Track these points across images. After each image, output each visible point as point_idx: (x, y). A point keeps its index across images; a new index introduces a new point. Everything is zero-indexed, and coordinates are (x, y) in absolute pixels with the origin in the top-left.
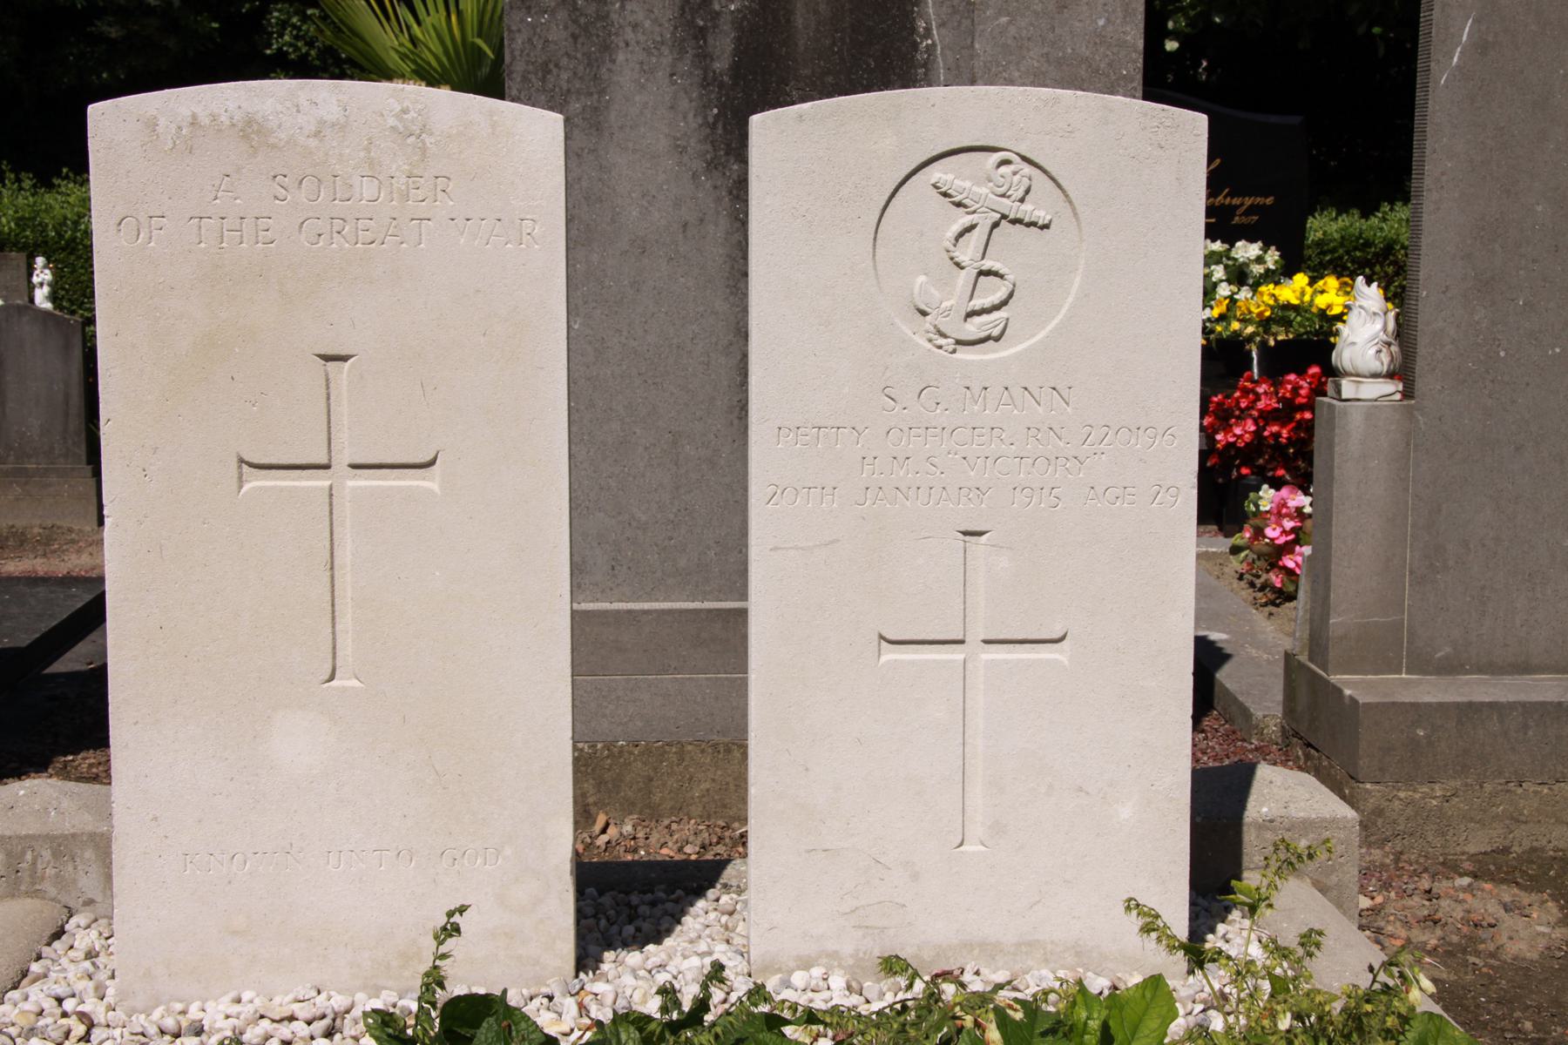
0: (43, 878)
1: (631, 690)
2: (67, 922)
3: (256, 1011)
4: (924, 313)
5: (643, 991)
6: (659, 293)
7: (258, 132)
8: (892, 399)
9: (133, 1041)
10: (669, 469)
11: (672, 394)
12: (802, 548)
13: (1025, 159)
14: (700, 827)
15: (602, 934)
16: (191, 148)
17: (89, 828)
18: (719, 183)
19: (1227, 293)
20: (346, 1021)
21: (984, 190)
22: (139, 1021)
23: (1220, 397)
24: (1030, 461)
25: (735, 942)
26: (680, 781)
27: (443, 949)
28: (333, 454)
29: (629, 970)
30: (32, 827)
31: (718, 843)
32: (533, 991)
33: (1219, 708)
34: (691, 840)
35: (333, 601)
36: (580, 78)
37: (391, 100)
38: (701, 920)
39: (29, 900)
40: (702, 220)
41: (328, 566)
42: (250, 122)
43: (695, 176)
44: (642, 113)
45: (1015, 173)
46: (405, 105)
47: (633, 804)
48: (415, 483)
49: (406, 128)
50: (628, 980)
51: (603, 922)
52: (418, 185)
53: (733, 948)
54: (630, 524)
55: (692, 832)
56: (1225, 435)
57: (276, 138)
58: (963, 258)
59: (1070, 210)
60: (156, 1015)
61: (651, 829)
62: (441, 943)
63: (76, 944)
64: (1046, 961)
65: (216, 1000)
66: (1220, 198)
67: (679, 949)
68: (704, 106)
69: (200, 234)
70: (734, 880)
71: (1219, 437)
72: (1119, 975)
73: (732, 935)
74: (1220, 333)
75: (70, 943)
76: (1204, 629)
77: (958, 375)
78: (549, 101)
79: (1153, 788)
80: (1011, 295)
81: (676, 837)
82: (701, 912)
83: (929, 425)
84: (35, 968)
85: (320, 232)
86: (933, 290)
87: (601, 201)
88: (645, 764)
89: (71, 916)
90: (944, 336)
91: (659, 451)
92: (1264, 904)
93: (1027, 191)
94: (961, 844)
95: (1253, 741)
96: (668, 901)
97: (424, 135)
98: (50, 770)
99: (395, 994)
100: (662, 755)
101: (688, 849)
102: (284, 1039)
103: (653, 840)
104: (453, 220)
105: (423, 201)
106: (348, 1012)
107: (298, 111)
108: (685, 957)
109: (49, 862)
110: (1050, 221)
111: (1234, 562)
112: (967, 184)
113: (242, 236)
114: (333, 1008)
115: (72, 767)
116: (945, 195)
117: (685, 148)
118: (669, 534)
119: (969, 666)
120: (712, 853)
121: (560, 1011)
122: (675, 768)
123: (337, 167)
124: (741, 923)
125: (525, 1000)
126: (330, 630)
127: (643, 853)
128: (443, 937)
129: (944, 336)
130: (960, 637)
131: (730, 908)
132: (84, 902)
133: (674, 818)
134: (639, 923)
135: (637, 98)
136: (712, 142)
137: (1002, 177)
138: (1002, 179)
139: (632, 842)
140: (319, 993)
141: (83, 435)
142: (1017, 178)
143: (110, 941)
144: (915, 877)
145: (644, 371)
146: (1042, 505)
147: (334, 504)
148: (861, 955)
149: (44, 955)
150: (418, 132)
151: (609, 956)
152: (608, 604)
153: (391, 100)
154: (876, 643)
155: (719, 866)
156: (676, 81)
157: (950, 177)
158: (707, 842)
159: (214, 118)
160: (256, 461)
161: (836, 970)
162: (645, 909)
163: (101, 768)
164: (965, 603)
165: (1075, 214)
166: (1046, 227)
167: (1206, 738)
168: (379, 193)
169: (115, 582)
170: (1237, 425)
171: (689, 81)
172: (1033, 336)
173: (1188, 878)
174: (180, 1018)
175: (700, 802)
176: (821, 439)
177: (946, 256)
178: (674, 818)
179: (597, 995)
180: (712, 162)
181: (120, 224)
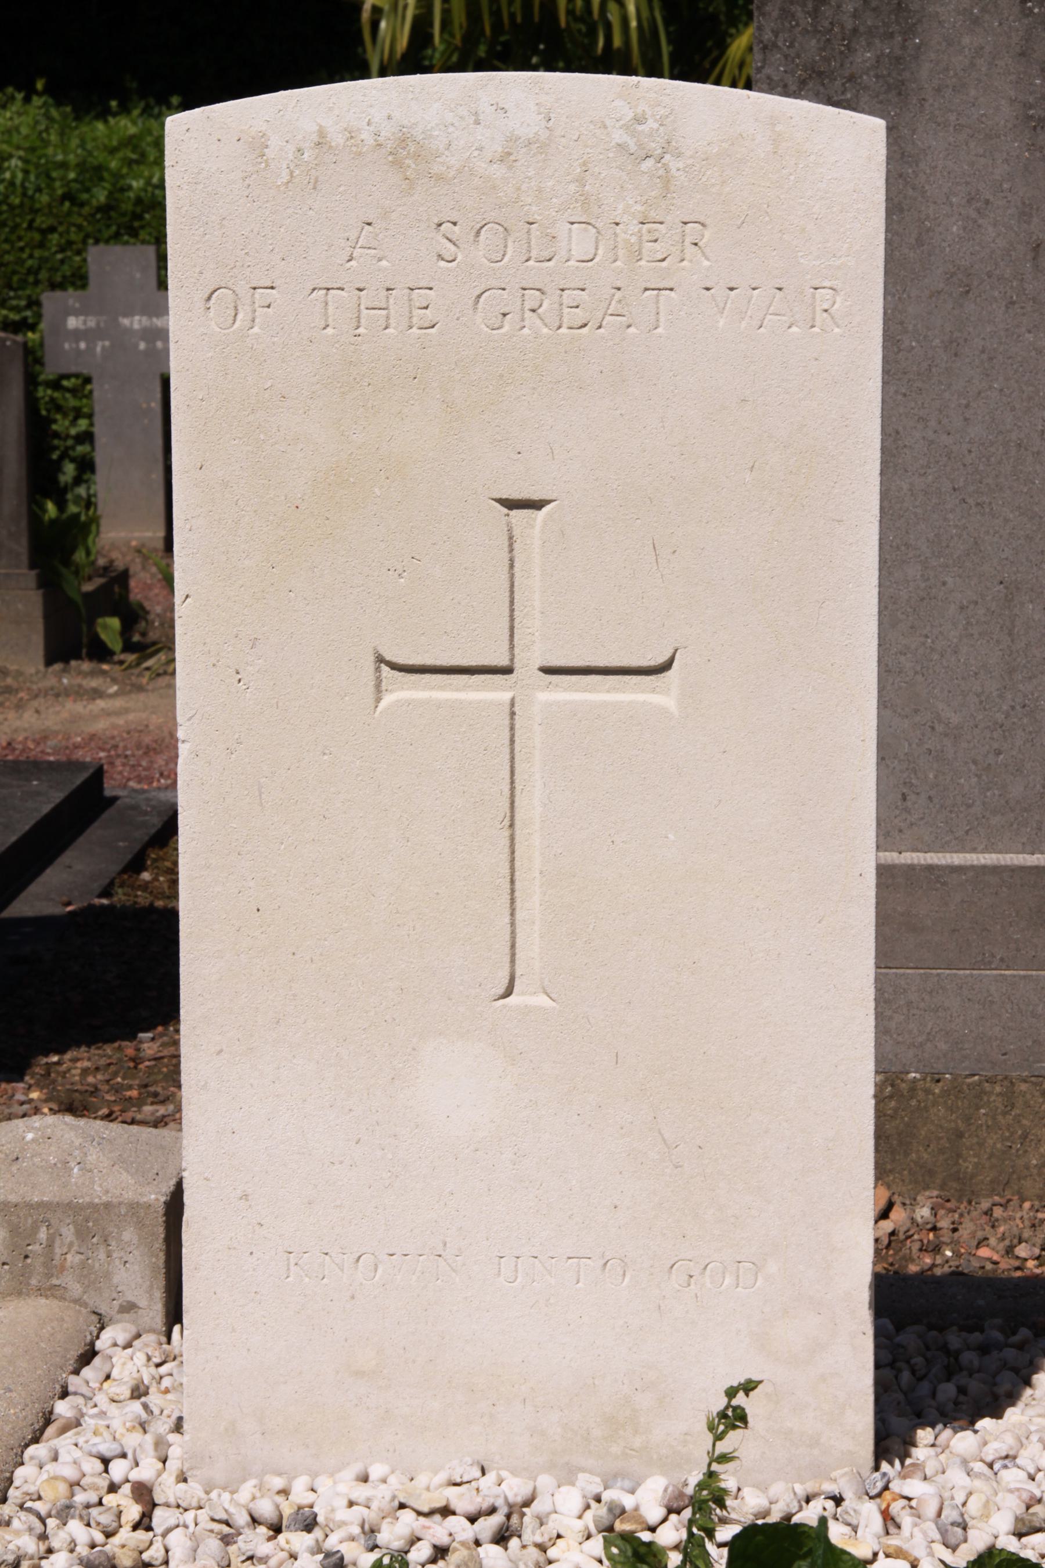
0: (62, 1268)
1: (931, 992)
2: (98, 1337)
3: (394, 1497)
5: (983, 1498)
6: (991, 359)
7: (417, 156)
9: (212, 1531)
10: (998, 642)
11: (1006, 520)
15: (905, 1394)
16: (316, 181)
17: (129, 1195)
20: (526, 1519)
22: (224, 1502)
26: (1007, 1139)
27: (722, 1447)
28: (516, 651)
29: (958, 1460)
30: (46, 1191)
32: (810, 1487)
34: (1026, 1234)
35: (512, 875)
36: (874, 10)
37: (617, 103)
39: (43, 1301)
41: (507, 822)
42: (403, 141)
44: (973, 65)
46: (639, 110)
47: (931, 1173)
48: (641, 697)
49: (640, 146)
50: (957, 1477)
51: (906, 1376)
52: (656, 235)
54: (933, 728)
55: (1027, 1223)
57: (443, 164)
60: (245, 1494)
61: (961, 1215)
62: (719, 1437)
63: (115, 1374)
65: (332, 1475)
69: (326, 314)
75: (106, 1369)
78: (823, 49)
81: (1002, 1229)
84: (63, 1408)
85: (505, 310)
87: (901, 210)
88: (951, 1110)
89: (102, 1328)
91: (982, 611)
96: (1007, 1345)
97: (667, 157)
98: (27, 1078)
99: (598, 1480)
101: (1022, 1251)
102: (438, 1543)
103: (964, 1233)
104: (708, 289)
105: (663, 260)
106: (527, 1503)
107: (477, 122)
109: (71, 1245)
113: (388, 317)
114: (506, 1498)
115: (58, 1073)
118: (996, 746)
121: (854, 1522)
122: (1000, 1118)
123: (534, 208)
125: (799, 1502)
126: (507, 920)
127: (949, 1253)
128: (722, 1428)
132: (121, 1306)
133: (997, 1199)
134: (963, 1379)
135: (966, 40)
139: (931, 1235)
140: (484, 1473)
141: (24, 524)
143: (163, 1370)
145: (961, 484)
147: (517, 726)
149: (71, 1389)
150: (660, 151)
151: (924, 1435)
152: (895, 855)
153: (618, 103)
156: (1031, 9)
159: (351, 134)
160: (401, 660)
162: (969, 1357)
163: (100, 1077)
168: (597, 249)
169: (193, 840)
174: (280, 1499)
178: (997, 1199)
179: (909, 1499)
181: (209, 298)
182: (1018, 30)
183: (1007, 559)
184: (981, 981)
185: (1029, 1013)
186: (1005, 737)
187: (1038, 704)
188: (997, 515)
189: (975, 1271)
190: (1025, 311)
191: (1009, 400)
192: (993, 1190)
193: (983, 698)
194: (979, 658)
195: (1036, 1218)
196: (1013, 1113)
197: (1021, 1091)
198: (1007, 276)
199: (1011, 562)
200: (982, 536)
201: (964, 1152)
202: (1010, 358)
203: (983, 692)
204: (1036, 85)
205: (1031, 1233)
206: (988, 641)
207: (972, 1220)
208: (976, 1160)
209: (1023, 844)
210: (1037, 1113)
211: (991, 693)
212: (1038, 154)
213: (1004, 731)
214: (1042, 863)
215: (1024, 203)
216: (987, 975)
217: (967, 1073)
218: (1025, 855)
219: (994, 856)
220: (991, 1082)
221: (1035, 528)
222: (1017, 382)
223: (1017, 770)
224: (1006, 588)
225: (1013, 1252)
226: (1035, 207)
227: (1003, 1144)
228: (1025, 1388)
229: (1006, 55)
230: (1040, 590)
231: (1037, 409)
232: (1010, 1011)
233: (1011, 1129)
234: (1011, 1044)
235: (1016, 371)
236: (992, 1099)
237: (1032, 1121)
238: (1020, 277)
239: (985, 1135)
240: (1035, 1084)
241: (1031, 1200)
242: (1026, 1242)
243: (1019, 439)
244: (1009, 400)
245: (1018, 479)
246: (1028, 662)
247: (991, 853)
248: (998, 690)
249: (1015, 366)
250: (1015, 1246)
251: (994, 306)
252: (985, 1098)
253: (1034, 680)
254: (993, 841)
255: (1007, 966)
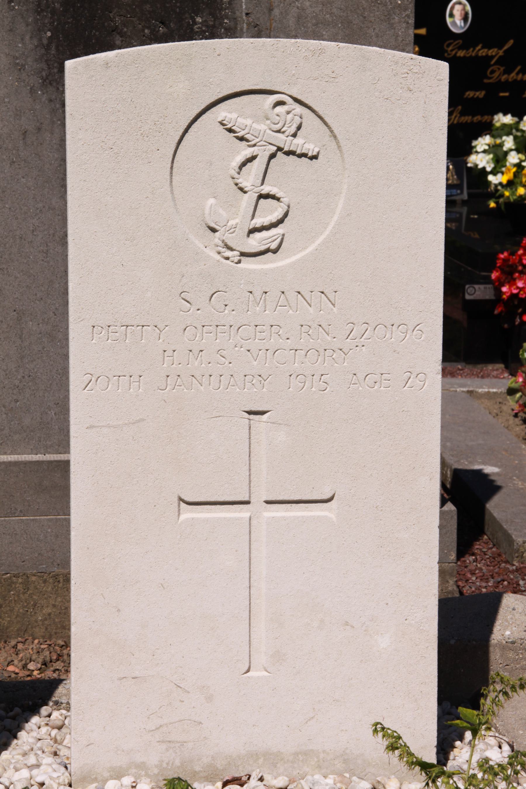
4: (214, 230)
8: (188, 302)
11: (16, 278)
12: (114, 427)
13: (296, 100)
14: (42, 646)
18: (54, 97)
19: (516, 161)
21: (262, 127)
23: (506, 254)
24: (303, 352)
25: (61, 753)
26: (26, 607)
31: (57, 660)
33: (488, 533)
34: (34, 657)
38: (34, 734)
40: (39, 129)
43: (32, 91)
45: (288, 113)
53: (59, 761)
55: (35, 651)
56: (510, 288)
58: (245, 184)
59: (334, 143)
64: (319, 767)
66: (513, 74)
67: (13, 761)
68: (39, 30)
70: (64, 698)
71: (504, 289)
72: (379, 779)
73: (60, 747)
74: (508, 197)
76: (480, 463)
77: (242, 282)
79: (407, 622)
80: (286, 215)
81: (21, 655)
82: (35, 728)
83: (218, 324)
86: (221, 211)
90: (231, 249)
92: (484, 727)
93: (299, 128)
94: (248, 671)
95: (515, 563)
96: (7, 718)
100: (10, 585)
108: (17, 770)
110: (318, 153)
111: (510, 401)
112: (248, 122)
116: (230, 130)
117: (23, 66)
118: (15, 397)
119: (253, 522)
120: (52, 669)
122: (21, 596)
124: (68, 736)
129: (231, 249)
130: (246, 499)
131: (60, 723)
133: (20, 639)
136: (46, 61)
137: (278, 115)
138: (278, 118)
142: (290, 116)
144: (210, 699)
146: (313, 389)
148: (165, 765)
154: (176, 504)
155: (55, 683)
156: (14, 7)
157: (234, 116)
158: (48, 659)
161: (143, 778)
164: (250, 470)
165: (339, 147)
166: (315, 157)
167: (475, 561)
170: (520, 279)
171: (25, 8)
172: (305, 248)
173: (436, 696)
175: (43, 625)
176: (128, 336)
177: (231, 182)
178: (20, 639)
180: (47, 78)
182: (7, 18)
183: (17, 298)
184: (10, 523)
185: (36, 539)
186: (20, 393)
187: (37, 375)
188: (11, 275)
189: (5, 679)
190: (20, 166)
191: (14, 214)
192: (19, 634)
193: (7, 372)
194: (5, 351)
195: (40, 648)
196: (28, 593)
197: (32, 581)
198: (10, 148)
199: (20, 300)
200: (3, 286)
201: (2, 615)
202: (14, 191)
203: (7, 369)
204: (19, 47)
205: (37, 656)
206: (9, 342)
207: (5, 651)
208: (9, 619)
209: (32, 449)
210: (41, 592)
211: (12, 369)
212: (22, 84)
213: (19, 390)
214: (2, 457)
215: (17, 109)
216: (13, 520)
217: (4, 573)
218: (33, 455)
219: (16, 456)
220: (16, 577)
221: (31, 282)
222: (18, 204)
223: (27, 410)
224: (18, 313)
225: (26, 667)
226: (22, 111)
227: (23, 610)
228: (14, 740)
229: (2, 30)
230: (35, 314)
231: (29, 219)
232: (26, 538)
233: (28, 602)
234: (27, 556)
235: (17, 199)
236: (17, 586)
237: (39, 596)
238: (17, 148)
239: (14, 605)
240: (40, 577)
241: (39, 639)
242: (34, 661)
243: (21, 234)
244: (14, 214)
245: (21, 256)
246: (31, 353)
247: (14, 455)
248: (15, 368)
249: (16, 196)
250: (28, 664)
251: (4, 164)
252: (13, 586)
253: (34, 362)
254: (15, 448)
255: (24, 515)
